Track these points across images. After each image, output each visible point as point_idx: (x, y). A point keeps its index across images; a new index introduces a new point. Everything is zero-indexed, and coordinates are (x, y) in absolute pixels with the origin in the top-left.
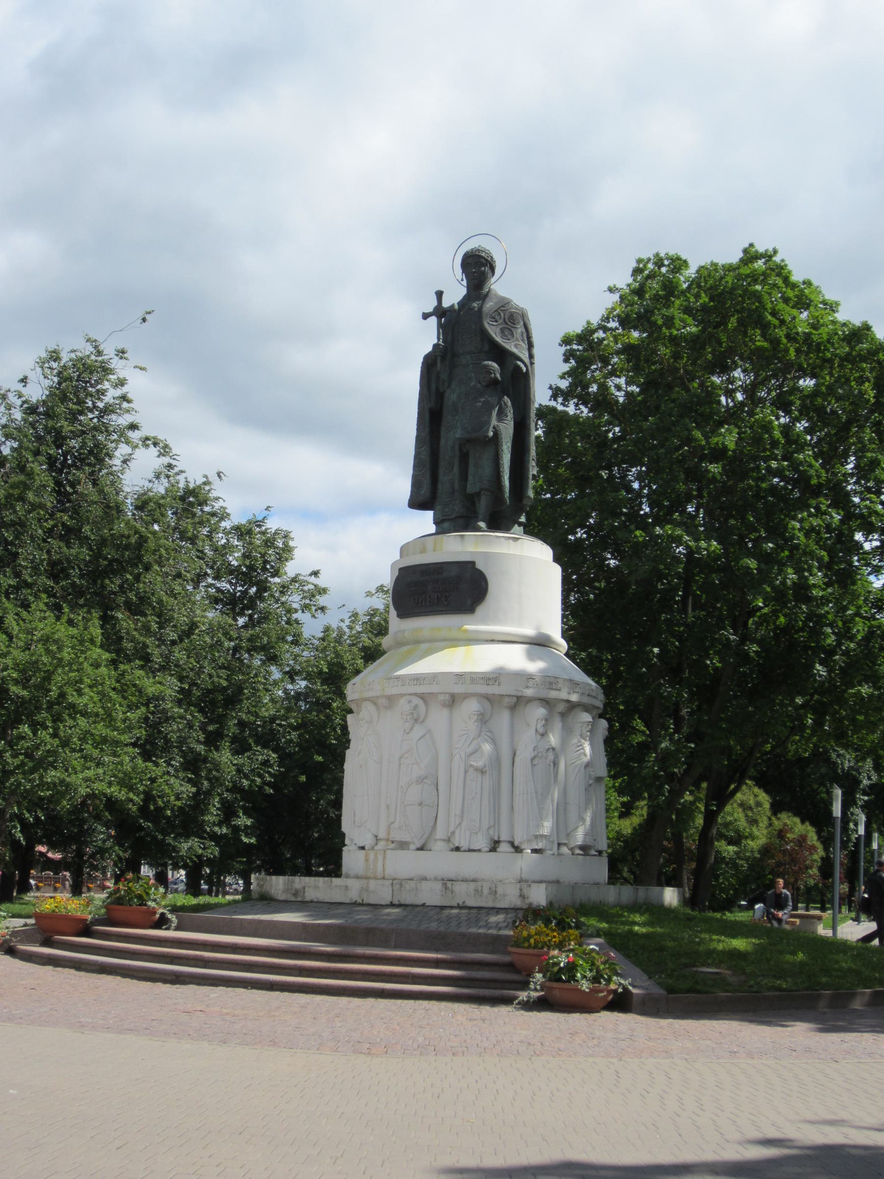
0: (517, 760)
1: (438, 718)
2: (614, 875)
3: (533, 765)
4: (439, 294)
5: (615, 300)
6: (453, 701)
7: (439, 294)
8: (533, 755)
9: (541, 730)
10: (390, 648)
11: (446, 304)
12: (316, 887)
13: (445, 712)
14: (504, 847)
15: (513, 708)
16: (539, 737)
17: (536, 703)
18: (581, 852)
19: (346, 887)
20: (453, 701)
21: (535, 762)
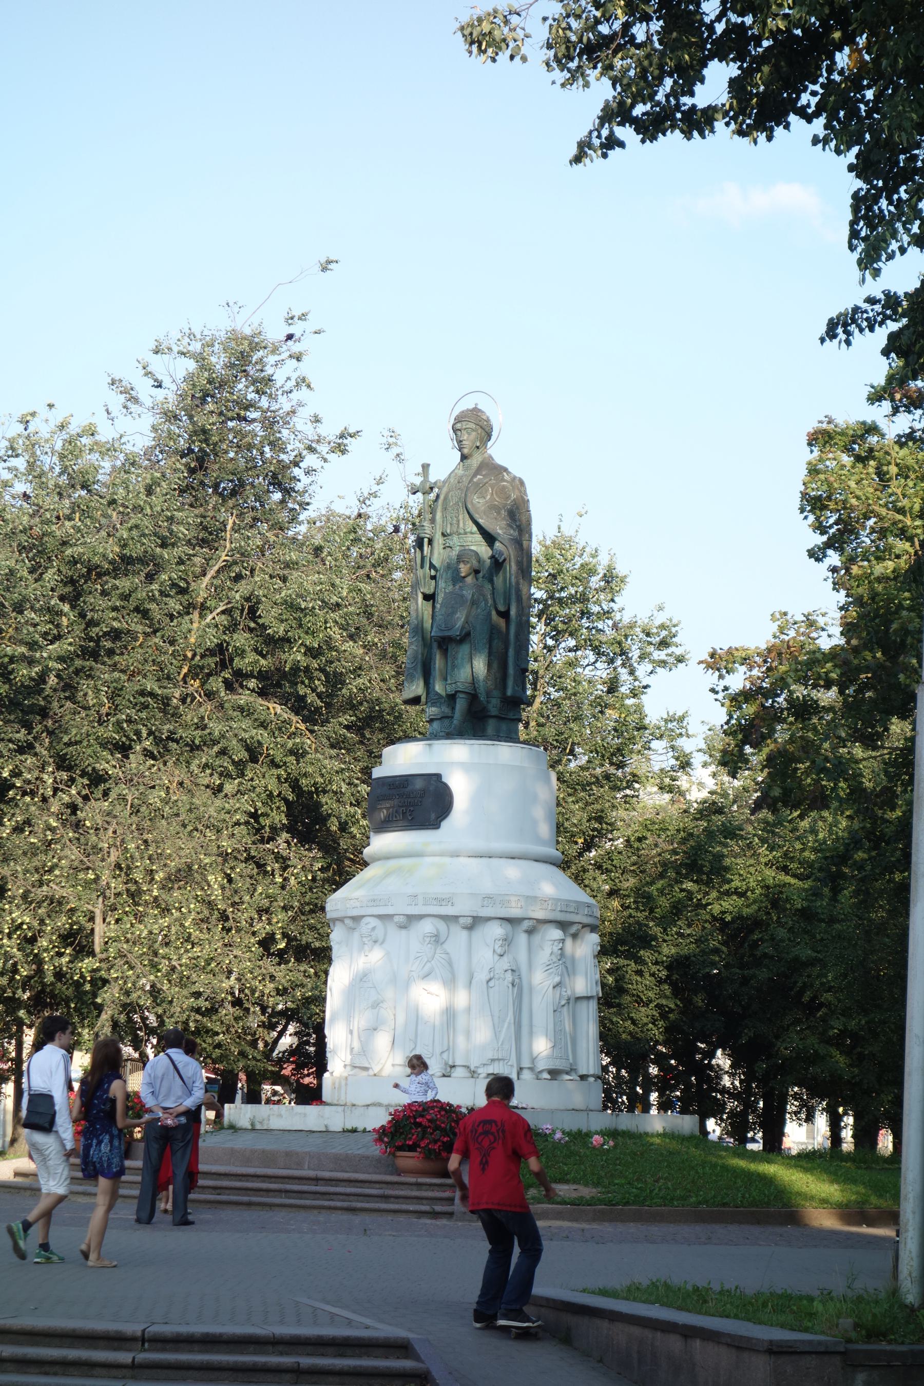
0: (474, 981)
1: (458, 938)
2: (609, 1102)
3: (488, 987)
4: (426, 467)
5: (819, 543)
6: (476, 922)
7: (426, 467)
8: (488, 978)
9: (499, 951)
10: (377, 858)
11: (432, 479)
12: (280, 1116)
13: (465, 933)
14: (459, 1072)
15: (530, 932)
16: (497, 957)
17: (498, 922)
18: (548, 1077)
19: (305, 1115)
20: (476, 922)
21: (491, 984)
